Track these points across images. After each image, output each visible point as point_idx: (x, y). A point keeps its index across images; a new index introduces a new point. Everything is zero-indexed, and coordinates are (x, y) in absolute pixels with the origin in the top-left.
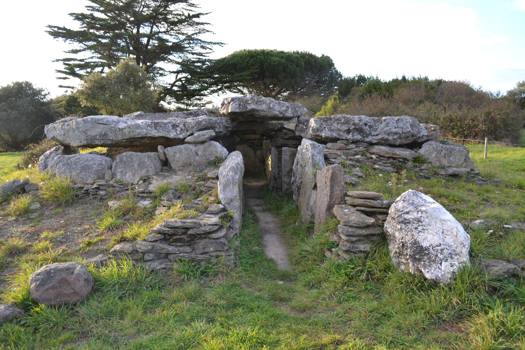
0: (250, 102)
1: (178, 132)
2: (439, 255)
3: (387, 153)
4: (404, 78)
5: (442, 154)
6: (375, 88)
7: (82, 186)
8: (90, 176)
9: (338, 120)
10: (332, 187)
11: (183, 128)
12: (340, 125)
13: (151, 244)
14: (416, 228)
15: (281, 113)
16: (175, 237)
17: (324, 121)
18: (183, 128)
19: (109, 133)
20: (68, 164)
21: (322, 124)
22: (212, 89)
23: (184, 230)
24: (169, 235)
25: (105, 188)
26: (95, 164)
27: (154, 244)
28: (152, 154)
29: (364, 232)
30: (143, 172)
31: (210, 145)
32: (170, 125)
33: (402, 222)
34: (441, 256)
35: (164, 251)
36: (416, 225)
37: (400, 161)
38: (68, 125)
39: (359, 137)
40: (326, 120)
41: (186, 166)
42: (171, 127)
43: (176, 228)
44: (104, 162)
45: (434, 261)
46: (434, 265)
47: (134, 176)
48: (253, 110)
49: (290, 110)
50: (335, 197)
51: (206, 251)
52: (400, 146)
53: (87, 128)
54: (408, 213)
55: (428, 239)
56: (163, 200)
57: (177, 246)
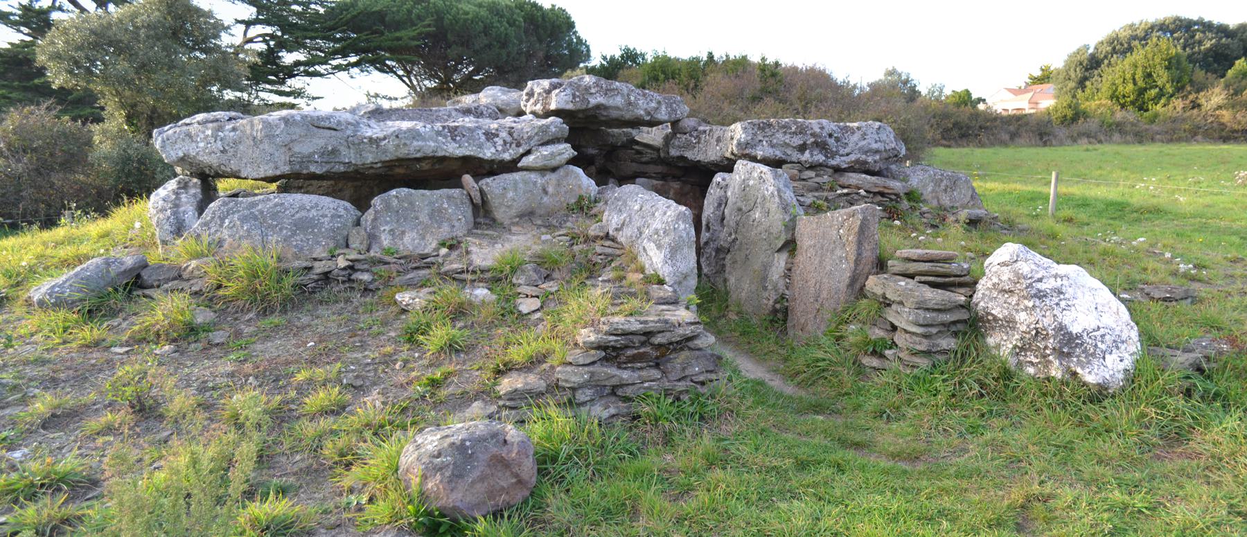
0: (593, 91)
1: (500, 148)
2: (1099, 344)
3: (876, 185)
4: (711, 56)
5: (943, 187)
6: (664, 72)
7: (309, 264)
8: (318, 243)
9: (786, 126)
10: (860, 243)
11: (509, 139)
12: (788, 136)
13: (586, 369)
14: (1057, 304)
15: (649, 113)
16: (629, 352)
17: (759, 128)
18: (509, 139)
19: (342, 148)
20: (256, 218)
21: (755, 134)
22: (334, 63)
23: (643, 338)
24: (614, 348)
25: (366, 266)
26: (324, 216)
27: (591, 369)
28: (456, 192)
29: (948, 318)
30: (445, 231)
31: (567, 175)
32: (480, 132)
33: (1035, 296)
34: (1103, 347)
35: (614, 381)
36: (1056, 300)
37: (891, 200)
38: (234, 129)
39: (820, 158)
40: (762, 128)
41: (527, 216)
42: (483, 138)
43: (632, 333)
44: (342, 212)
45: (1093, 355)
46: (1095, 362)
47: (423, 238)
48: (598, 107)
49: (663, 107)
50: (864, 261)
51: (687, 373)
53: (294, 137)
54: (1040, 280)
55: (1077, 322)
56: (520, 285)
57: (633, 369)
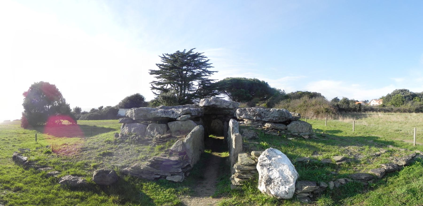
39: (259, 118)
52: (280, 123)
